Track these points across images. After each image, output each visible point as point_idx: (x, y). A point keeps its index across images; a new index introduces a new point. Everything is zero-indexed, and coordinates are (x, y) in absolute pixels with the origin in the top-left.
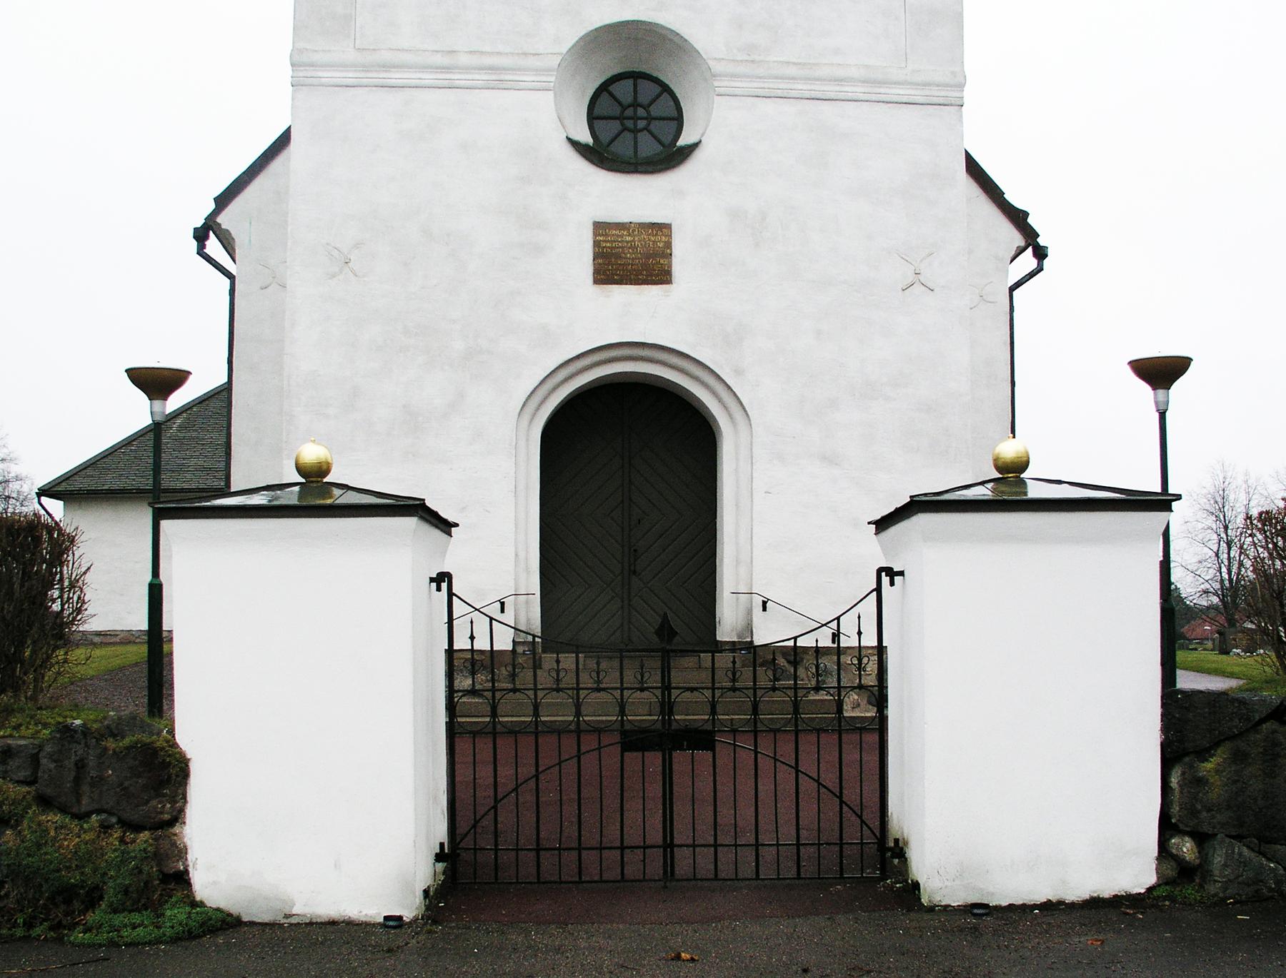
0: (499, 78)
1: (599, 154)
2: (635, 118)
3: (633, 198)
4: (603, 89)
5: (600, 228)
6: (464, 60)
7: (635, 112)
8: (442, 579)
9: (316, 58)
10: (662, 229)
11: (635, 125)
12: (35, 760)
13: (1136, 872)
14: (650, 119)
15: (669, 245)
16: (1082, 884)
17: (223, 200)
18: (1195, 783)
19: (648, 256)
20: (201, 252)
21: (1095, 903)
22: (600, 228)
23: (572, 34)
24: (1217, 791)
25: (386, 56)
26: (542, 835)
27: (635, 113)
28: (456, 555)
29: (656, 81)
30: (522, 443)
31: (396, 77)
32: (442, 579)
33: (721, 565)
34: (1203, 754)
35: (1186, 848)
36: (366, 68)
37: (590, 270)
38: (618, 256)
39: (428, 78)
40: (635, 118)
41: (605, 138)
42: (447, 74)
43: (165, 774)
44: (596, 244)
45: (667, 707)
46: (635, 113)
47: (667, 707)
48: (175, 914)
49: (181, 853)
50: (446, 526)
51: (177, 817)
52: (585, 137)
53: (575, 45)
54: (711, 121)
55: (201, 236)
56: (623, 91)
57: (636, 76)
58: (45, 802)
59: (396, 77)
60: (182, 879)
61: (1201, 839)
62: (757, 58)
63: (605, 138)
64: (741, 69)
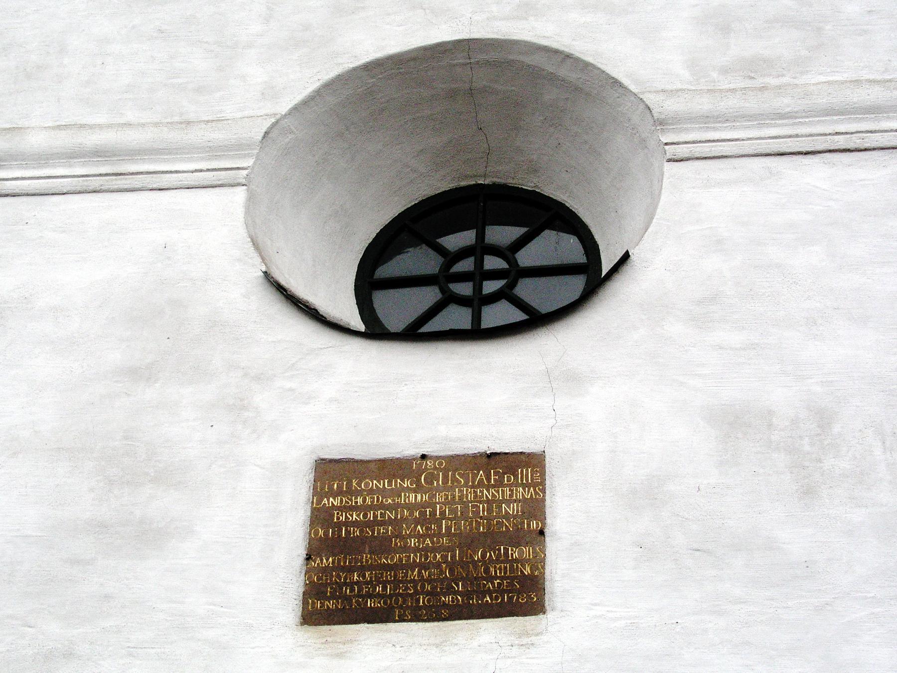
2: (480, 275)
3: (444, 400)
5: (332, 473)
7: (479, 263)
10: (517, 469)
11: (478, 288)
15: (536, 508)
19: (469, 542)
22: (332, 473)
23: (303, 79)
26: (50, 124)
27: (477, 225)
33: (413, 47)
38: (383, 546)
40: (480, 275)
44: (320, 517)
46: (477, 225)
53: (306, 103)
54: (677, 231)
62: (773, 81)
64: (731, 103)
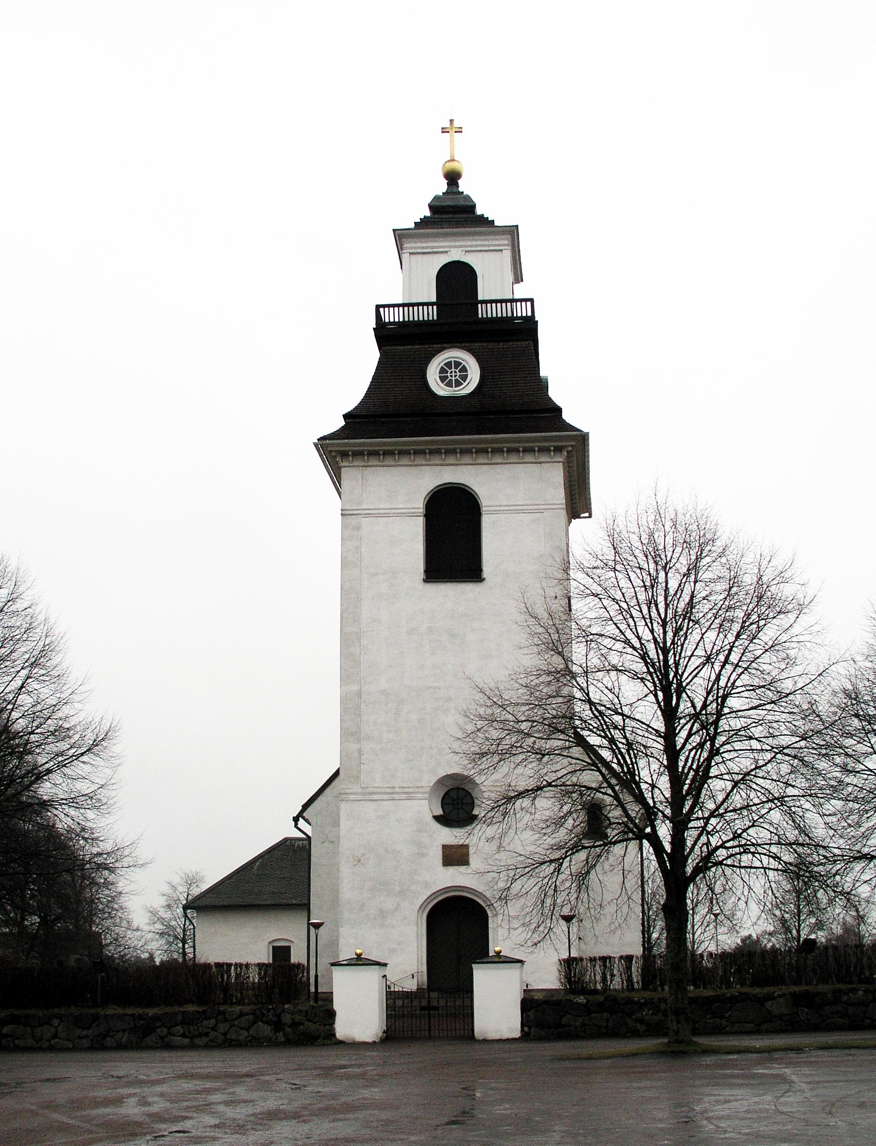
0: (410, 796)
1: (444, 820)
4: (447, 794)
6: (397, 790)
8: (385, 976)
9: (349, 791)
12: (306, 1012)
13: (517, 1034)
14: (463, 804)
16: (507, 1035)
17: (306, 807)
18: (528, 1016)
20: (296, 826)
21: (508, 1040)
23: (434, 779)
24: (532, 1017)
25: (370, 790)
28: (388, 971)
29: (463, 789)
30: (420, 924)
31: (375, 797)
32: (385, 976)
33: (508, 968)
34: (529, 1010)
35: (526, 1029)
36: (364, 794)
37: (441, 861)
39: (385, 797)
41: (447, 811)
42: (392, 794)
43: (332, 1014)
45: (429, 1002)
47: (429, 1002)
48: (333, 1040)
49: (334, 1030)
50: (385, 965)
51: (334, 1023)
52: (439, 812)
55: (296, 819)
56: (454, 795)
57: (458, 789)
58: (309, 1020)
59: (375, 797)
60: (334, 1035)
61: (530, 1028)
63: (447, 811)
